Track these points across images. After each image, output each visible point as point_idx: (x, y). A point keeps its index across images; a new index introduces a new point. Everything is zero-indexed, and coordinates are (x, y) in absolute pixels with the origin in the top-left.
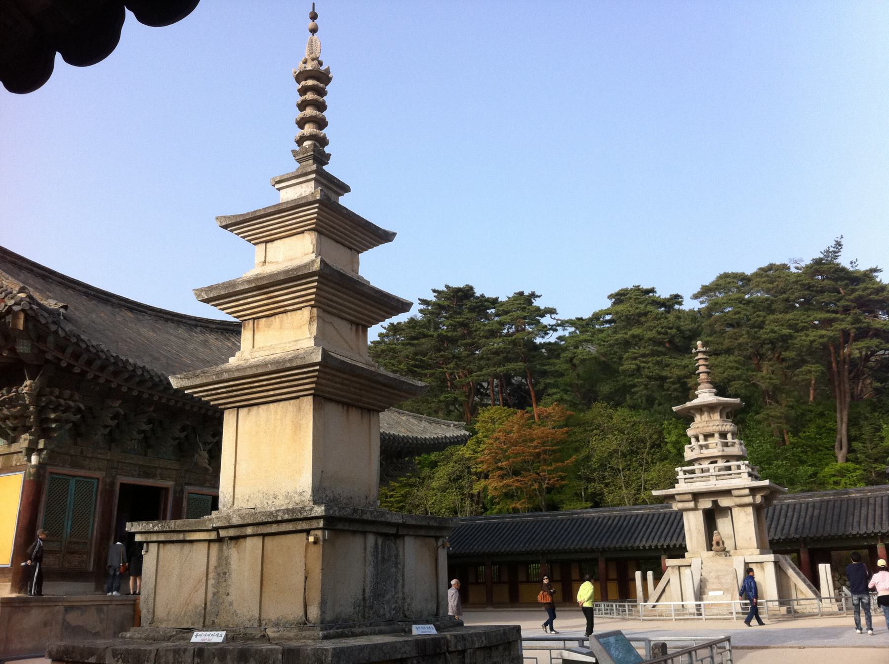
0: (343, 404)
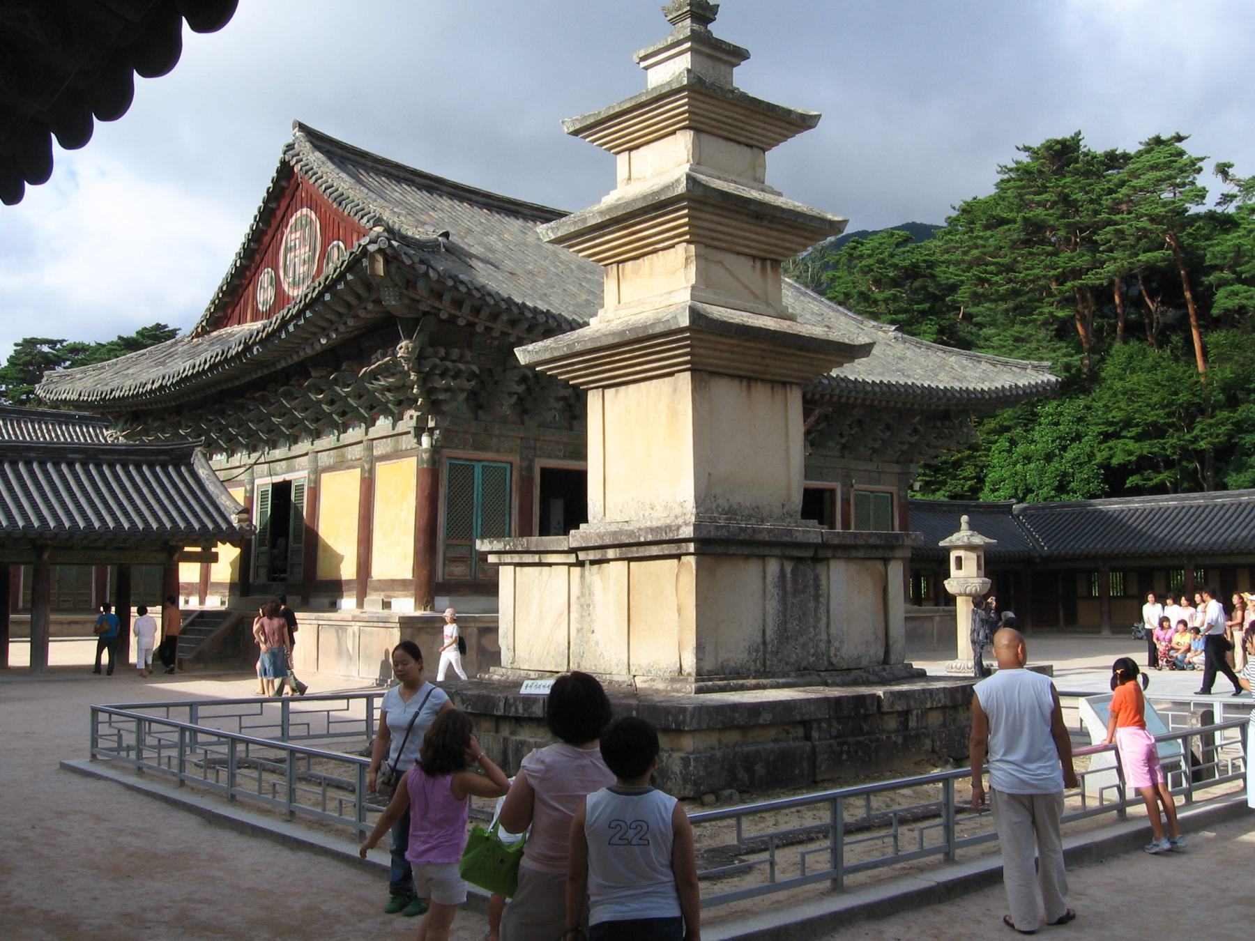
0: (740, 378)
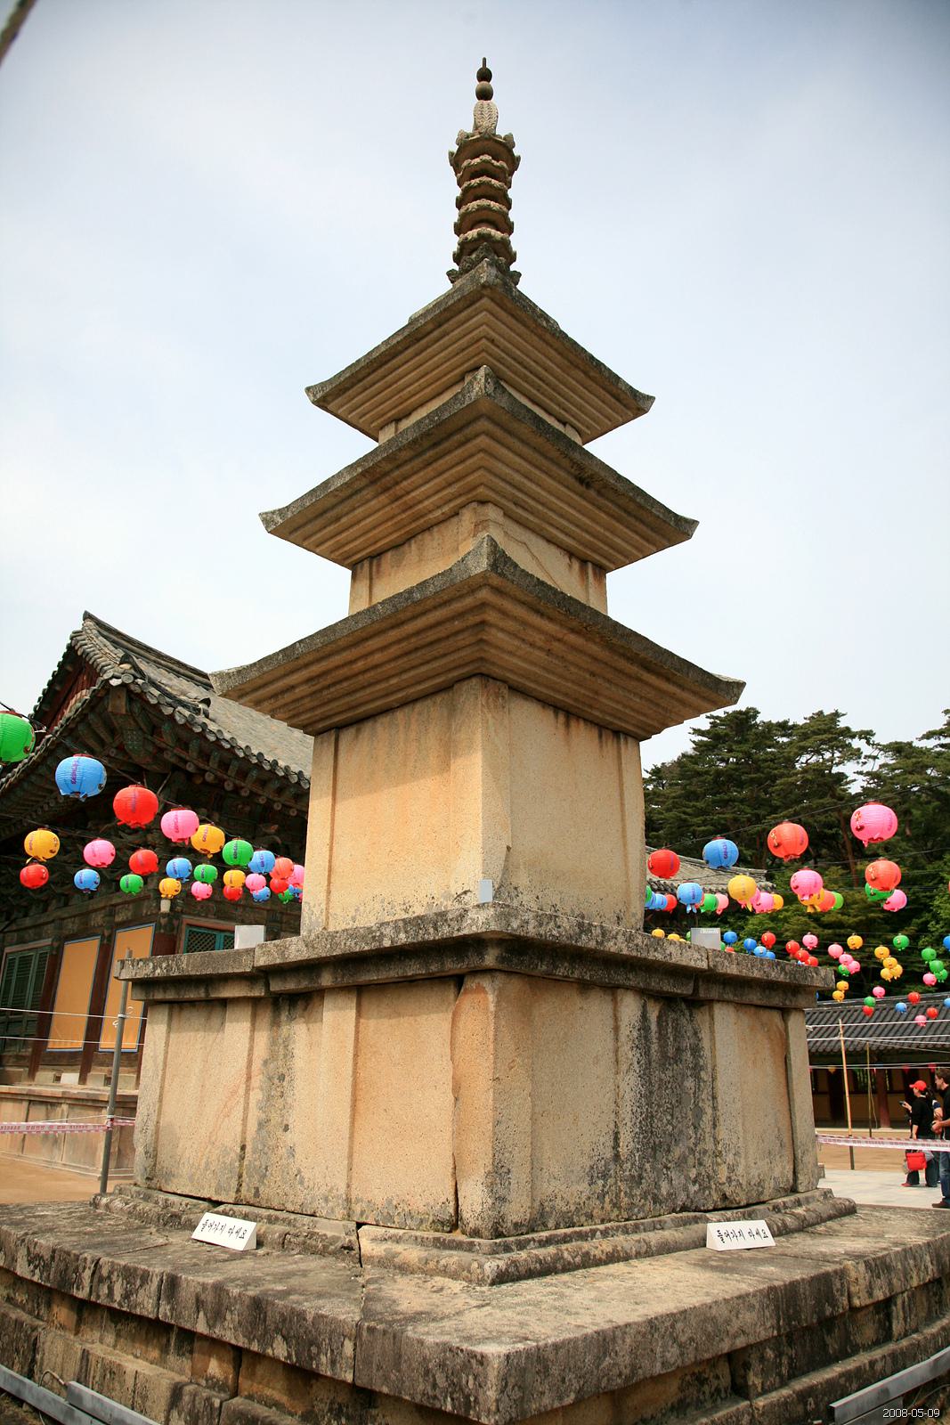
0: (556, 708)
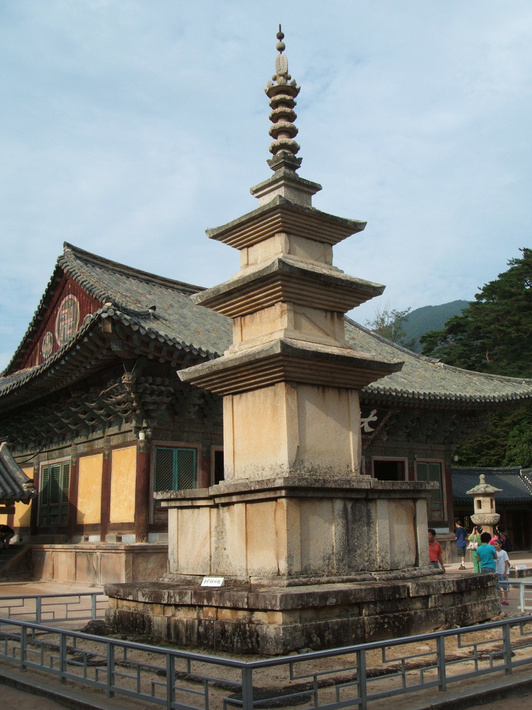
0: (318, 386)
